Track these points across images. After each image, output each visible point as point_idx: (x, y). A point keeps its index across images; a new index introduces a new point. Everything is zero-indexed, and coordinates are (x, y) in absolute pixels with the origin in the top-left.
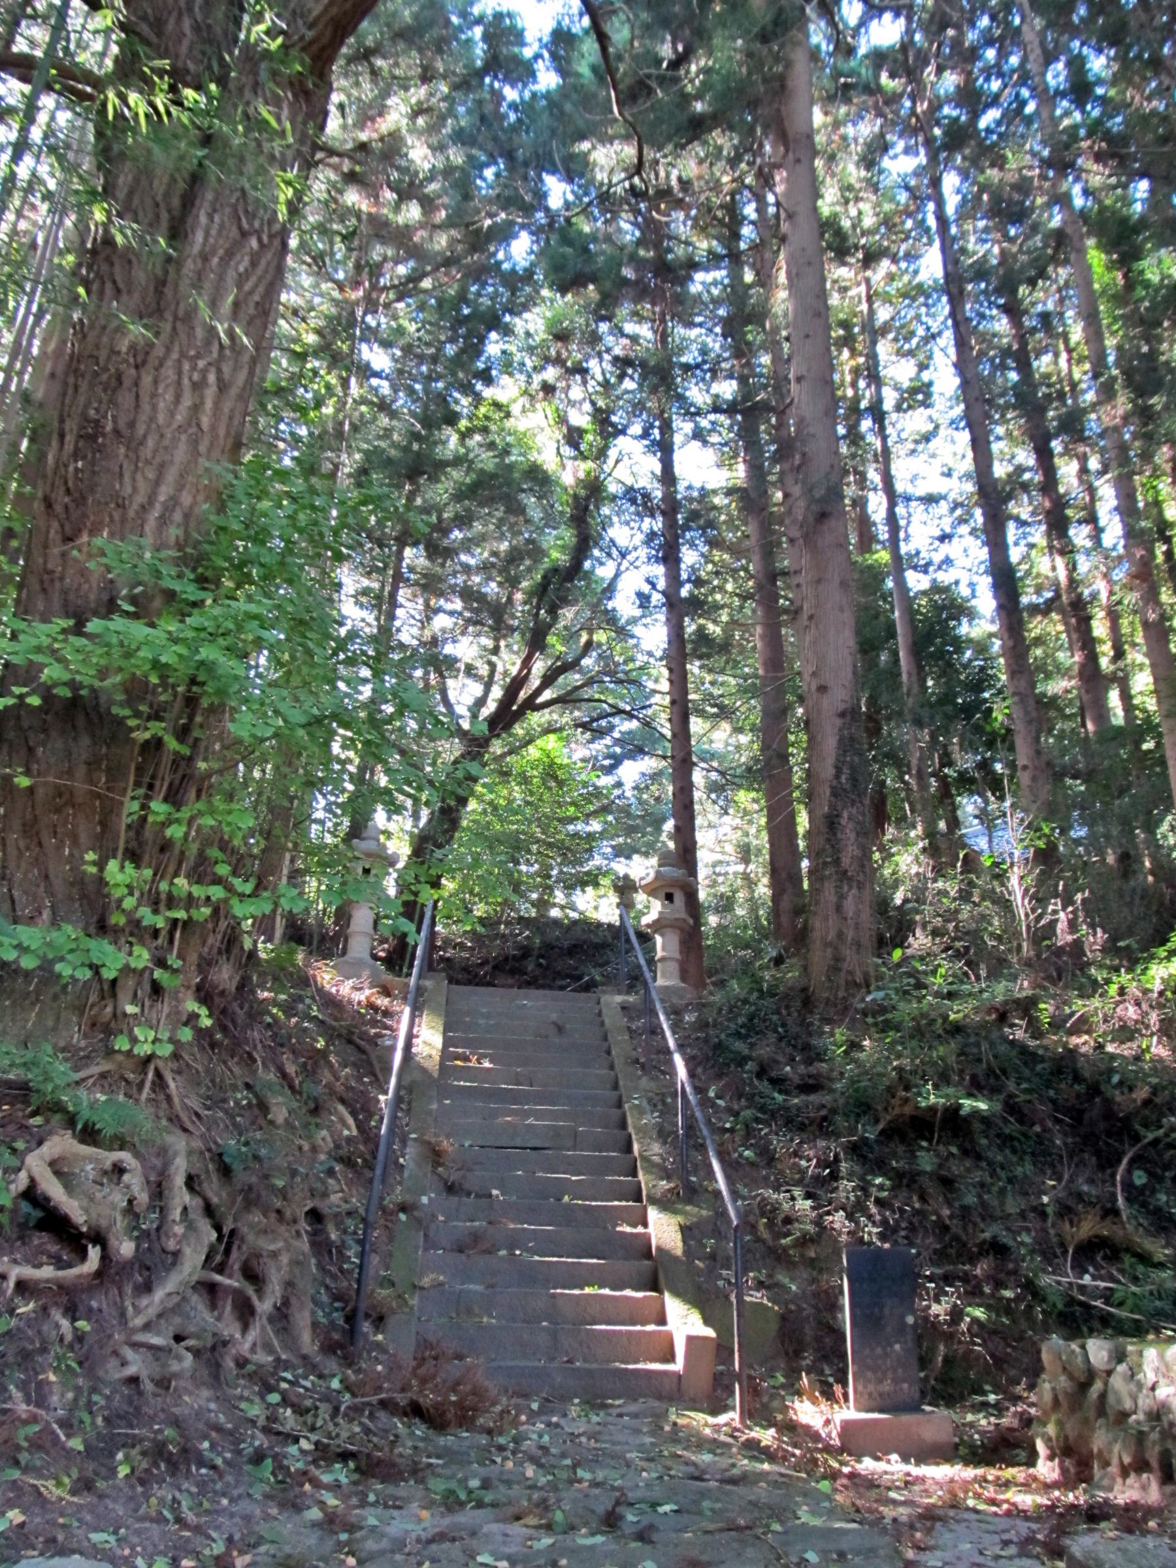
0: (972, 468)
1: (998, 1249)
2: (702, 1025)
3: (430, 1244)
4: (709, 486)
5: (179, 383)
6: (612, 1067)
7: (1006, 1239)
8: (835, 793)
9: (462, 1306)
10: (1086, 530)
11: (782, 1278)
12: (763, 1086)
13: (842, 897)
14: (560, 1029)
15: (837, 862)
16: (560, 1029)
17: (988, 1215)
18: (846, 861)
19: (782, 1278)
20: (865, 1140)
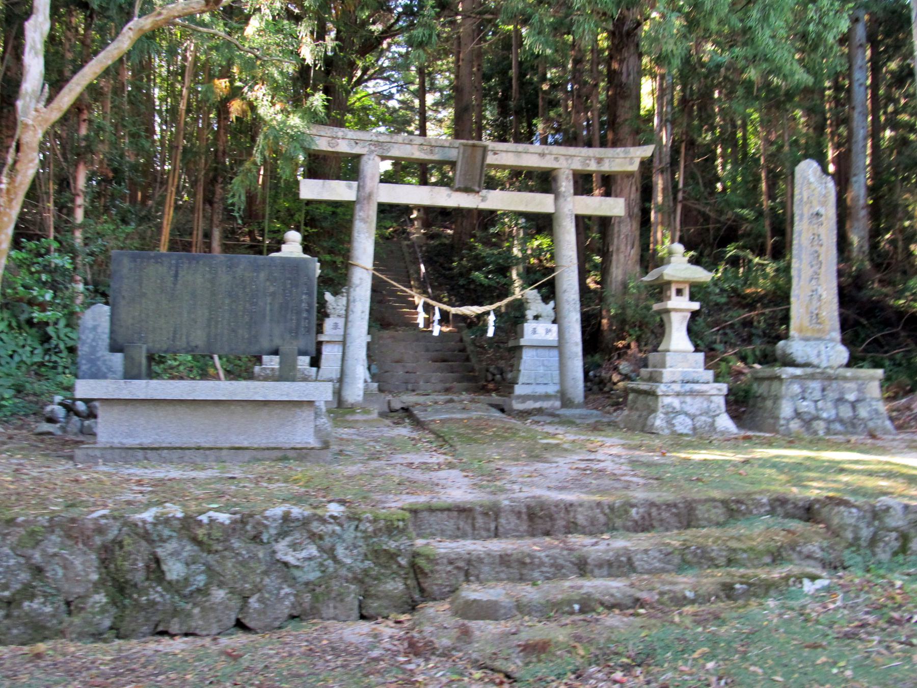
2: (427, 251)
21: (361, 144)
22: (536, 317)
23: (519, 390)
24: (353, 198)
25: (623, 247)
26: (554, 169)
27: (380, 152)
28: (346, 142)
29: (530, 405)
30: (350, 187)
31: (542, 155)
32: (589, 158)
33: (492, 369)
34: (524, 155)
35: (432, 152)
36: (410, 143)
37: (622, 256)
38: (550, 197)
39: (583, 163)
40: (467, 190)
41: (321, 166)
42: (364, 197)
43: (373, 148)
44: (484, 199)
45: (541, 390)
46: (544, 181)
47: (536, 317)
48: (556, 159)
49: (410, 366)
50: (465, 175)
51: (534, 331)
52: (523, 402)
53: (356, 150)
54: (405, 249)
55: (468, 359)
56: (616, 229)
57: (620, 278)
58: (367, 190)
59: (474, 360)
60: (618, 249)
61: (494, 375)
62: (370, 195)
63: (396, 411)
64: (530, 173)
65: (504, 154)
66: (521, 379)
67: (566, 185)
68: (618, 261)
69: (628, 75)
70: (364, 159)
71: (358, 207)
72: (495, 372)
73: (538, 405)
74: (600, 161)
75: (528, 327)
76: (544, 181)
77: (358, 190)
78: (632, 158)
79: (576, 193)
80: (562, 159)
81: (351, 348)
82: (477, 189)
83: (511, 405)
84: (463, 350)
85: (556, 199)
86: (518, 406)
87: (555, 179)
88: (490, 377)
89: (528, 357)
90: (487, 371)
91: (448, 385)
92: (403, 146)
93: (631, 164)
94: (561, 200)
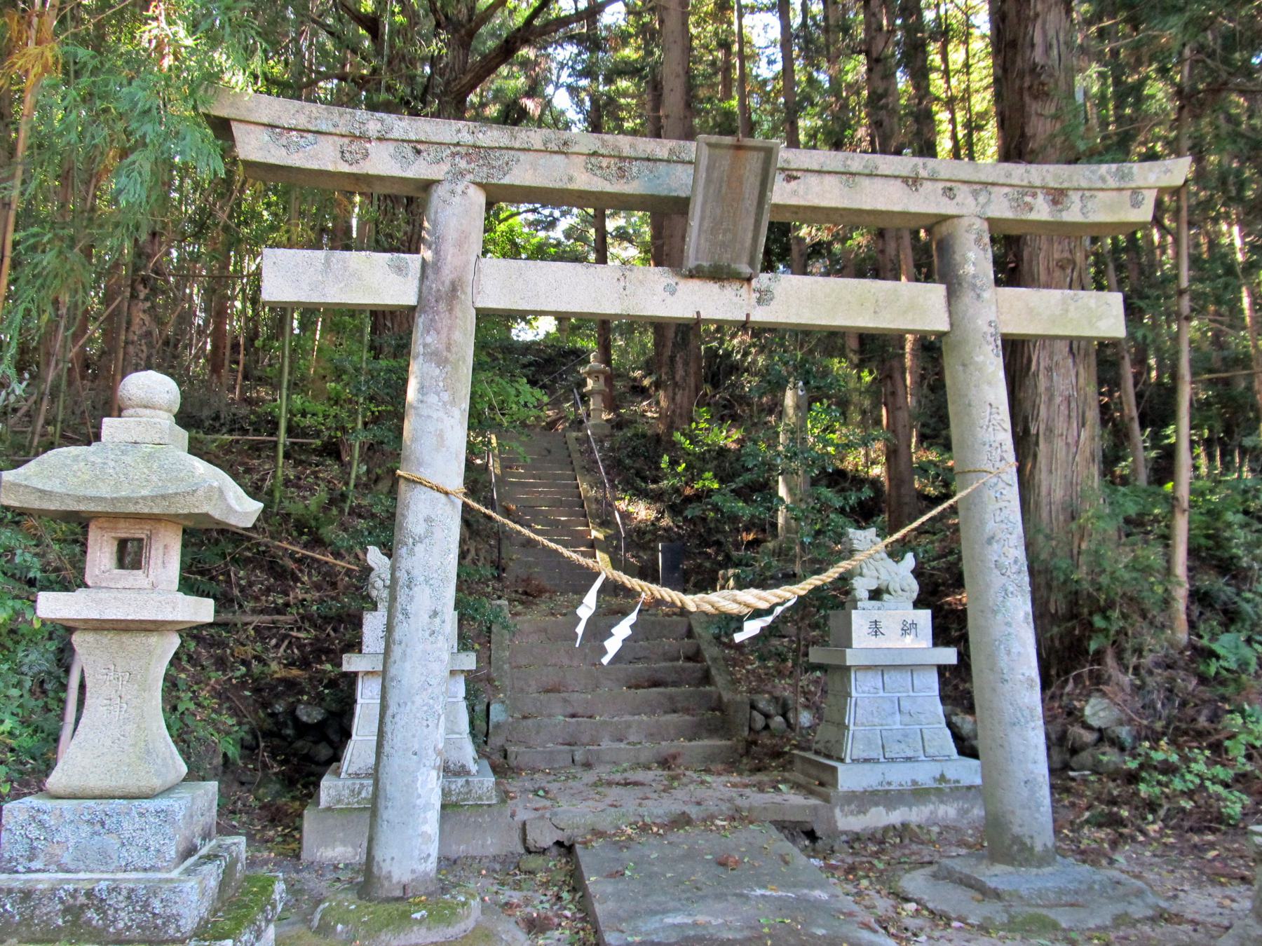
0: (779, 37)
1: (718, 544)
2: (612, 449)
3: (512, 545)
4: (703, 316)
5: (1069, 416)
6: (573, 470)
7: (723, 540)
8: (674, 345)
9: (528, 565)
10: (538, 145)
11: (641, 554)
12: (638, 481)
13: (675, 394)
14: (549, 452)
15: (674, 378)
16: (549, 452)
17: (718, 531)
18: (678, 378)
19: (641, 554)
20: (674, 504)
21: (430, 153)
22: (876, 595)
23: (849, 778)
24: (411, 300)
25: (1060, 425)
26: (943, 219)
27: (482, 175)
28: (391, 147)
29: (879, 817)
30: (400, 270)
31: (913, 182)
32: (1031, 190)
33: (763, 702)
34: (866, 182)
35: (622, 174)
36: (564, 150)
37: (1059, 444)
38: (935, 292)
39: (1019, 204)
40: (718, 274)
41: (323, 211)
42: (439, 293)
43: (463, 164)
44: (764, 297)
45: (900, 776)
46: (918, 251)
47: (876, 595)
48: (949, 192)
49: (578, 700)
50: (714, 231)
51: (876, 629)
52: (862, 811)
53: (419, 170)
54: (573, 446)
55: (706, 678)
56: (1043, 383)
57: (1059, 494)
58: (447, 274)
59: (720, 679)
60: (1050, 430)
61: (767, 716)
62: (454, 289)
63: (543, 851)
64: (883, 228)
65: (813, 180)
66: (853, 749)
67: (976, 260)
68: (1051, 456)
69: (1048, 47)
70: (439, 192)
71: (421, 321)
72: (771, 709)
73: (896, 817)
74: (1057, 196)
75: (859, 620)
76: (918, 251)
77: (423, 276)
78: (1136, 191)
79: (998, 283)
80: (963, 192)
81: (401, 720)
82: (745, 269)
83: (831, 821)
84: (695, 656)
85: (951, 296)
86: (849, 822)
87: (945, 247)
88: (759, 721)
89: (862, 689)
90: (753, 707)
91: (666, 747)
92: (544, 159)
93: (1136, 204)
94: (967, 298)
